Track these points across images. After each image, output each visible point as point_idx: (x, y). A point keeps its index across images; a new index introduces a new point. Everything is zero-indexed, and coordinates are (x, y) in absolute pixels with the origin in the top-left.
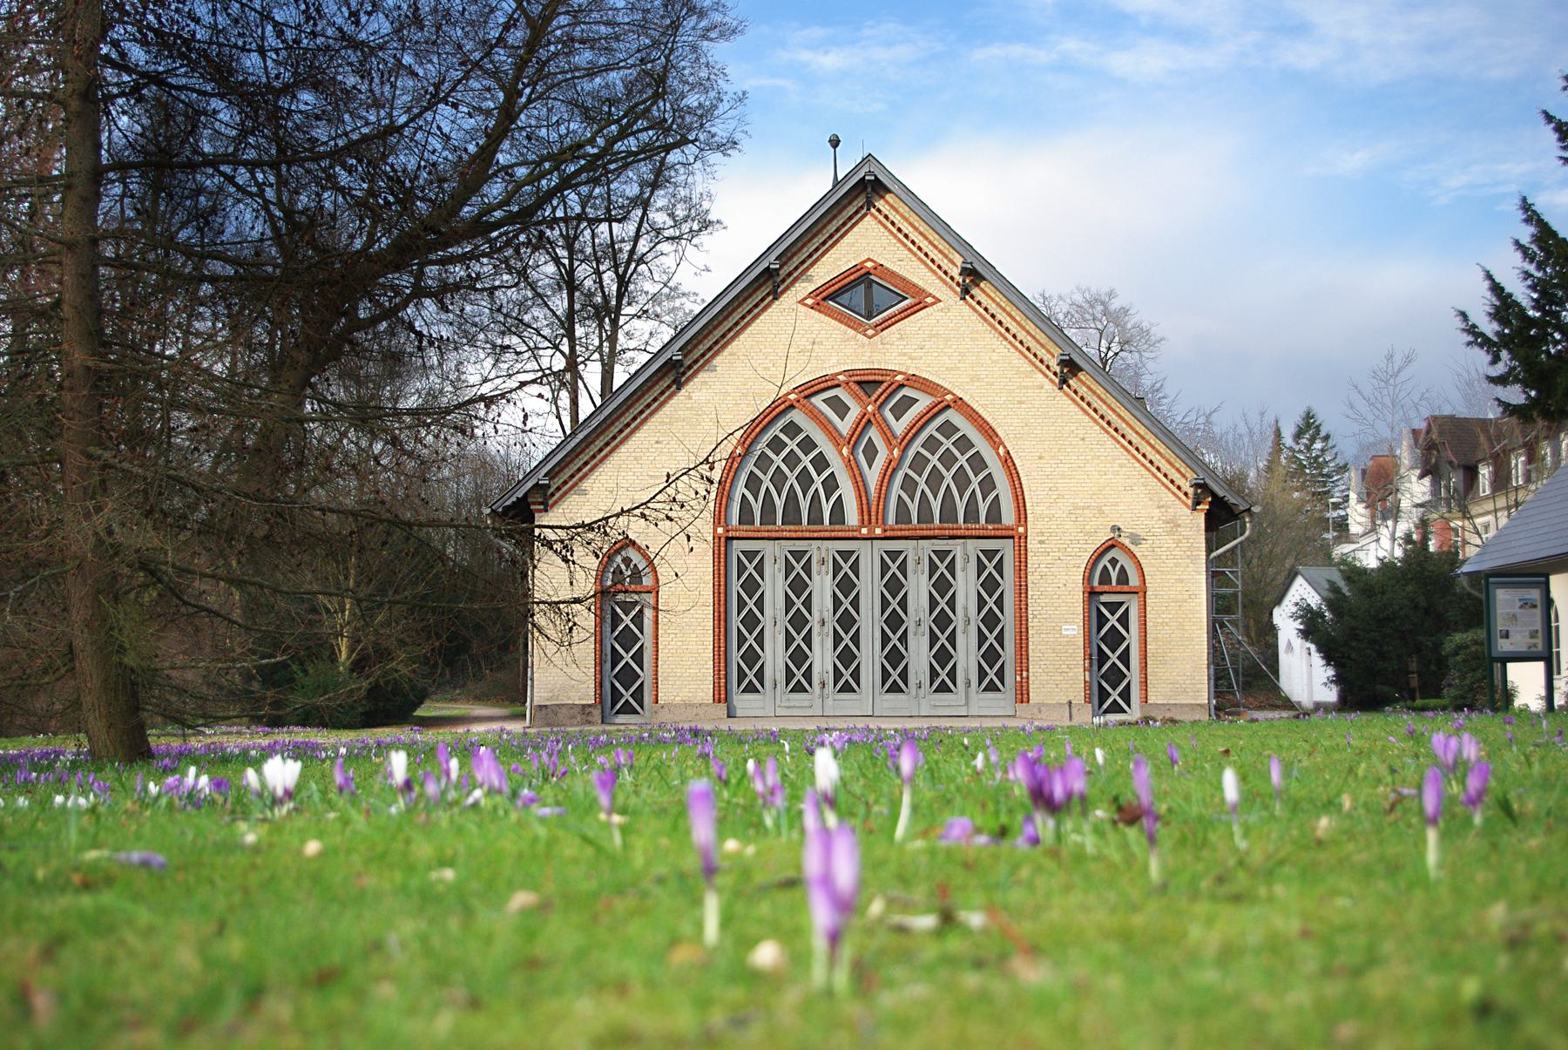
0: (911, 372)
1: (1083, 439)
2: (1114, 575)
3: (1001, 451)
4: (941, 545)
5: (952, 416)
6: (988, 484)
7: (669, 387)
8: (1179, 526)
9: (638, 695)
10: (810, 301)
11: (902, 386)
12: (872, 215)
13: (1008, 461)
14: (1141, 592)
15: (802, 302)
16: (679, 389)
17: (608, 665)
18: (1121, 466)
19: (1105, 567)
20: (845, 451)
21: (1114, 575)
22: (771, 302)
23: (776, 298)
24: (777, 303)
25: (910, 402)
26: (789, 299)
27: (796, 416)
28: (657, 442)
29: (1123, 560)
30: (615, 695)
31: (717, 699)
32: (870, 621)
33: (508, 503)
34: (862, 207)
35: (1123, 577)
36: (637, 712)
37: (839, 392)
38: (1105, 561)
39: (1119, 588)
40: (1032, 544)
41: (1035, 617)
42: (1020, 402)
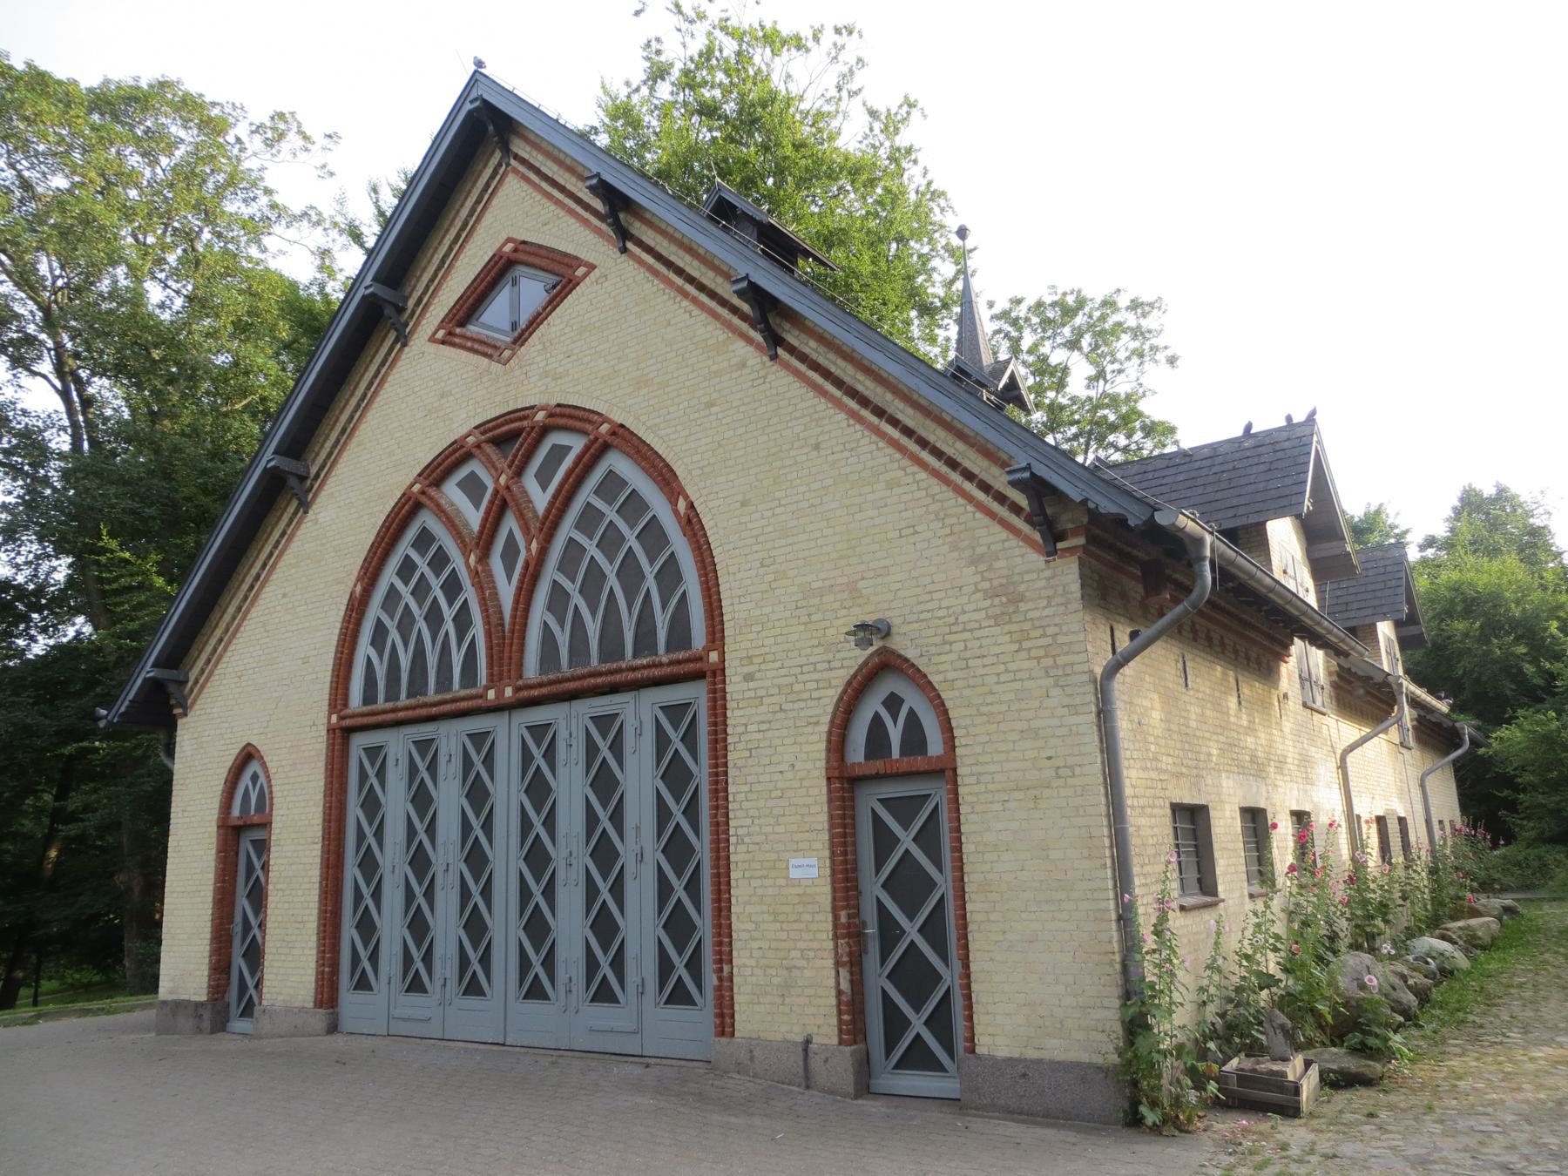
0: (553, 402)
1: (817, 447)
2: (895, 734)
3: (682, 505)
4: (424, 730)
5: (618, 463)
6: (670, 575)
7: (295, 513)
8: (1022, 599)
9: (941, 1022)
10: (581, 271)
11: (545, 430)
12: (516, 171)
13: (692, 524)
14: (946, 771)
15: (592, 267)
16: (306, 512)
17: (874, 948)
18: (890, 486)
19: (877, 719)
20: (472, 559)
21: (895, 734)
22: (401, 350)
23: (404, 345)
24: (407, 349)
25: (560, 452)
26: (420, 341)
27: (426, 519)
28: (284, 596)
29: (913, 700)
30: (895, 1024)
31: (319, 1003)
32: (506, 859)
33: (123, 709)
34: (500, 165)
35: (914, 738)
36: (940, 1068)
37: (474, 467)
38: (873, 705)
39: (906, 764)
40: (735, 686)
41: (740, 842)
42: (710, 405)
